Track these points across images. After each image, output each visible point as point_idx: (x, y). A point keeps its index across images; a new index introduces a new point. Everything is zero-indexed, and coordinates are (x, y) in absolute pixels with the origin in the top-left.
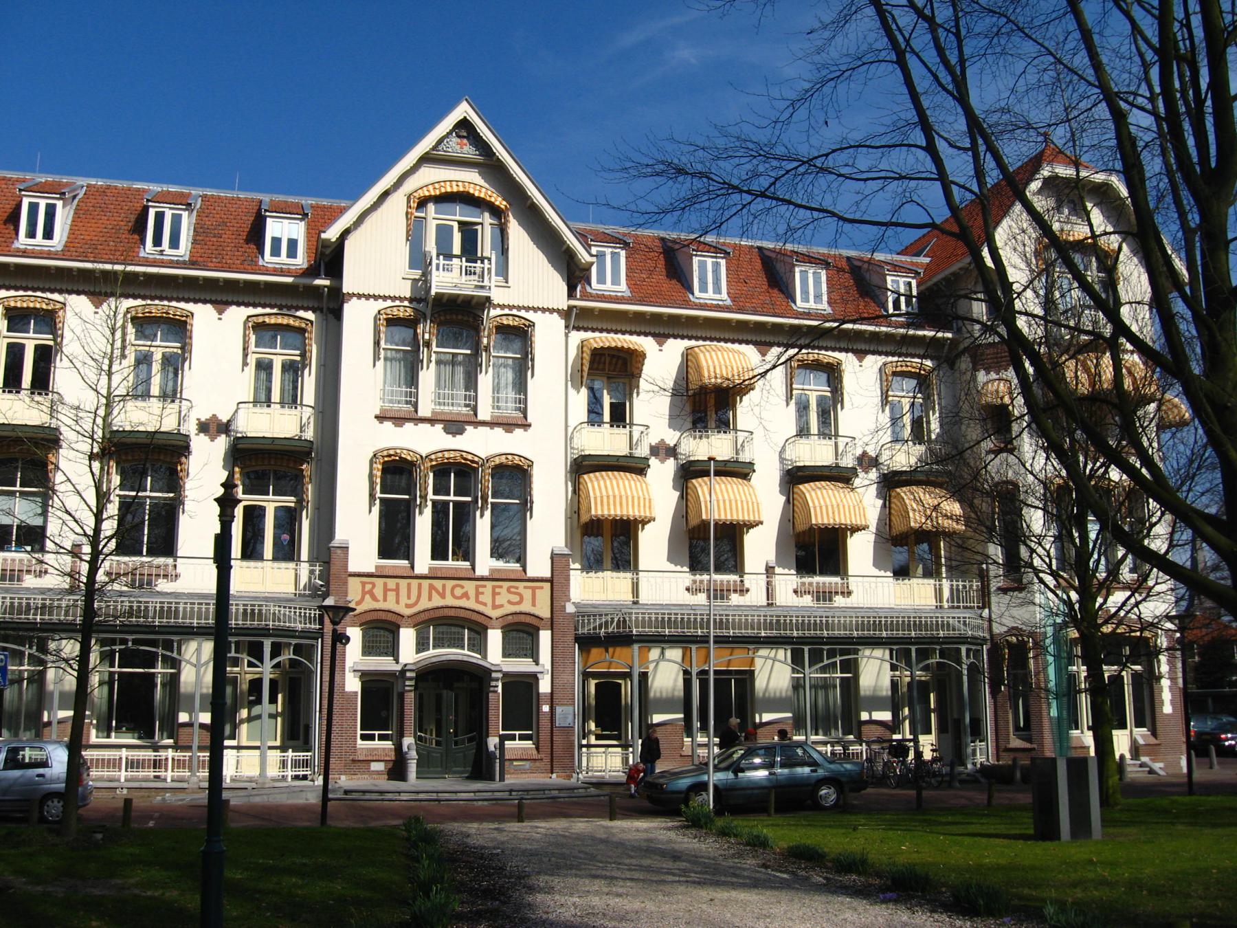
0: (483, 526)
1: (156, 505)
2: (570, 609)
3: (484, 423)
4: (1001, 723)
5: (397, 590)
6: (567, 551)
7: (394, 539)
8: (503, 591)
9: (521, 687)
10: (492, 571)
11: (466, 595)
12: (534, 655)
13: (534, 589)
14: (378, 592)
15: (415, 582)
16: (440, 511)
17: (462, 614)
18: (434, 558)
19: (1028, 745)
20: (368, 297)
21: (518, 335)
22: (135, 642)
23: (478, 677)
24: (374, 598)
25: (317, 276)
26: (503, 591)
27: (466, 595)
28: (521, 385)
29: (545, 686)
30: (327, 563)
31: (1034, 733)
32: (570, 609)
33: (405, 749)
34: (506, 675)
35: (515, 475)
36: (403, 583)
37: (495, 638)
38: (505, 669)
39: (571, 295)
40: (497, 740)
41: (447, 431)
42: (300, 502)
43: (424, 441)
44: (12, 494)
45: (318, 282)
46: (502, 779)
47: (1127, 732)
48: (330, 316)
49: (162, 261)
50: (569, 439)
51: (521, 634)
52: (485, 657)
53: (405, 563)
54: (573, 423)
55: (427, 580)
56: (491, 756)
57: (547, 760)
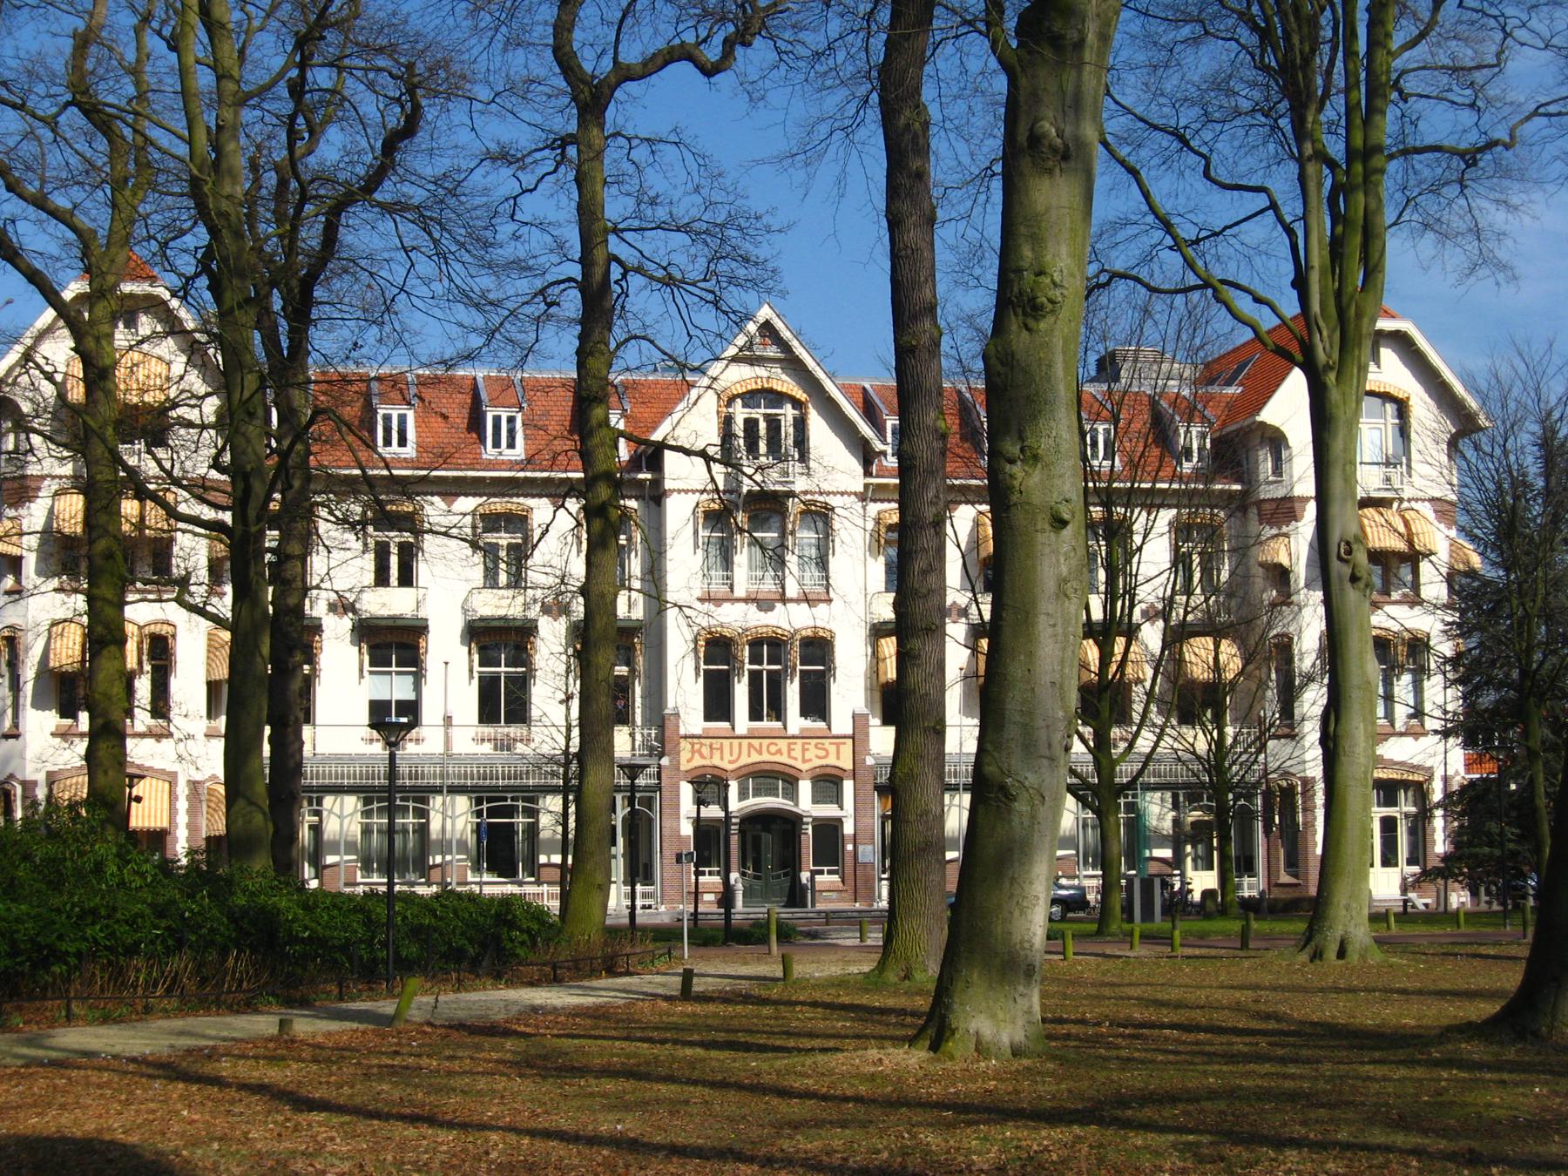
0: (793, 692)
1: (510, 678)
2: (870, 761)
3: (792, 600)
4: (1273, 861)
5: (721, 749)
6: (866, 711)
7: (717, 705)
8: (812, 747)
9: (833, 826)
10: (802, 730)
11: (779, 752)
12: (838, 800)
13: (838, 745)
14: (705, 751)
15: (736, 742)
16: (755, 677)
17: (777, 768)
18: (708, 717)
19: (1294, 881)
20: (687, 491)
21: (820, 516)
22: (505, 799)
23: (788, 824)
24: (702, 756)
25: (640, 471)
26: (812, 747)
27: (779, 752)
28: (822, 563)
29: (848, 829)
30: (662, 727)
31: (1301, 870)
32: (870, 761)
33: (732, 882)
34: (815, 819)
35: (819, 648)
36: (726, 742)
37: (805, 787)
38: (815, 814)
39: (867, 473)
40: (808, 874)
41: (760, 609)
42: (632, 671)
43: (736, 618)
44: (390, 673)
45: (641, 476)
46: (813, 905)
47: (1397, 870)
48: (652, 504)
49: (503, 463)
50: (868, 605)
51: (828, 784)
52: (797, 805)
53: (726, 725)
54: (871, 591)
55: (741, 743)
56: (803, 888)
57: (851, 891)
